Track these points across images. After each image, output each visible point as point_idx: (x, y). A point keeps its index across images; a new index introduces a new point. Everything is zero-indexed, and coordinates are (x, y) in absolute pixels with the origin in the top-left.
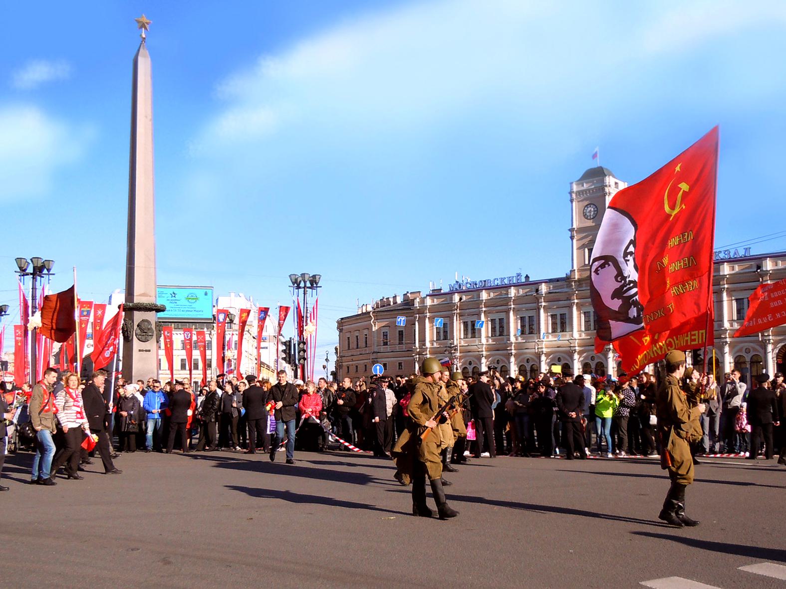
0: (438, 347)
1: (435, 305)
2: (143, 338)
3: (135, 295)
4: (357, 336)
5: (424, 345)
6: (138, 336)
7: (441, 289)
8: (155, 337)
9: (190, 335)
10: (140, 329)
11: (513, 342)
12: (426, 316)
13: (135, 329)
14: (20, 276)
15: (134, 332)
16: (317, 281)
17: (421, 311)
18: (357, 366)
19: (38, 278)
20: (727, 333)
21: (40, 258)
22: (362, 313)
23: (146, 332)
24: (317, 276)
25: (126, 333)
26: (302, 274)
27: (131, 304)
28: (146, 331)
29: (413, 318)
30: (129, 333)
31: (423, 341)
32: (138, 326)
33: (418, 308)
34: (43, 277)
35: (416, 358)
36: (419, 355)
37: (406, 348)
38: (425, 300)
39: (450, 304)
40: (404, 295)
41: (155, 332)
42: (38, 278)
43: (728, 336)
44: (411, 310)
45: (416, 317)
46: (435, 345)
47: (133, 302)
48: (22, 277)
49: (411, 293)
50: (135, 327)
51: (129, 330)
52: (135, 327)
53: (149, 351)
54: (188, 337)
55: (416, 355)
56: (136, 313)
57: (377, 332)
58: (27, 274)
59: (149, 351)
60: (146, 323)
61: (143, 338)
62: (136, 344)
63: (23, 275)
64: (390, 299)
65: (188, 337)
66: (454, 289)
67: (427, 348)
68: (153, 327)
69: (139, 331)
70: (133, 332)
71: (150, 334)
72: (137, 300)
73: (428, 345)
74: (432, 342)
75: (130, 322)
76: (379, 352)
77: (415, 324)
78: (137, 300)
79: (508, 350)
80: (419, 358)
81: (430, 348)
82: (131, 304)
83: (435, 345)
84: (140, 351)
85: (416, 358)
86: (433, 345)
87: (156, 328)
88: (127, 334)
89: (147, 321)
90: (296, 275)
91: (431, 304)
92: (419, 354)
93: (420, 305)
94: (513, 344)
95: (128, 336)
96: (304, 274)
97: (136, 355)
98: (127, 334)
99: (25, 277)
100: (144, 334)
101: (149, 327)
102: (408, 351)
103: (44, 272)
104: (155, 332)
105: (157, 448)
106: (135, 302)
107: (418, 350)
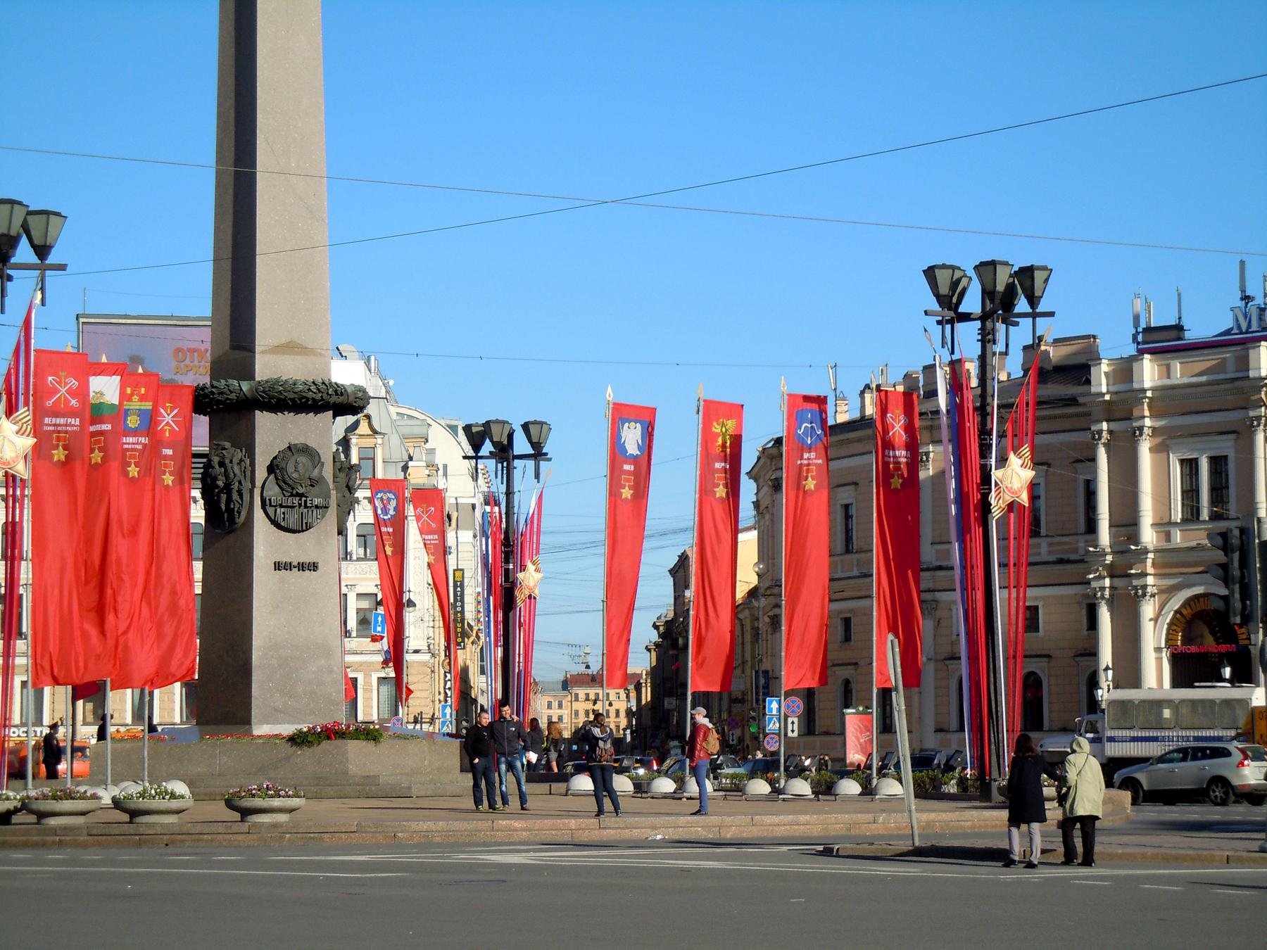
0: (1192, 549)
1: (1173, 387)
2: (293, 519)
3: (258, 349)
4: (846, 507)
5: (1134, 537)
6: (271, 511)
7: (1179, 328)
8: (332, 513)
9: (393, 503)
10: (285, 484)
11: (1150, 547)
12: (1141, 429)
13: (259, 483)
14: (939, 323)
15: (257, 492)
16: (1037, 294)
17: (1122, 409)
18: (847, 622)
19: (1000, 327)
20: (1149, 562)
21: (58, 214)
22: (863, 418)
23: (300, 495)
24: (1037, 273)
25: (224, 497)
26: (983, 264)
27: (245, 386)
28: (301, 490)
29: (1088, 435)
30: (235, 496)
31: (1127, 523)
32: (271, 469)
33: (1107, 397)
34: (1016, 324)
35: (1103, 589)
36: (1111, 576)
37: (1050, 553)
38: (1135, 365)
39: (1238, 384)
40: (1025, 348)
41: (333, 493)
42: (1000, 327)
43: (1150, 570)
44: (1080, 405)
45: (1100, 432)
46: (1178, 537)
47: (250, 376)
48: (948, 327)
49: (1056, 341)
50: (261, 473)
51: (235, 486)
52: (261, 473)
53: (314, 567)
54: (385, 511)
55: (1101, 578)
56: (263, 420)
57: (933, 484)
58: (966, 317)
59: (314, 567)
60: (302, 459)
61: (293, 519)
62: (266, 542)
63: (951, 322)
64: (968, 365)
65: (385, 511)
66: (1254, 327)
67: (1146, 551)
68: (328, 472)
69: (273, 492)
70: (252, 492)
71: (316, 501)
72: (269, 366)
73: (1148, 536)
74: (1164, 526)
75: (239, 454)
76: (940, 568)
77: (1093, 459)
78: (269, 366)
79: (1130, 575)
80: (1112, 588)
81: (1156, 551)
82: (245, 386)
83: (1178, 537)
84: (278, 566)
85: (1103, 589)
86: (1168, 537)
87: (335, 477)
88: (229, 500)
89: (306, 450)
90: (954, 268)
91: (1159, 383)
92: (1113, 572)
93: (1112, 389)
94: (1151, 555)
95: (230, 511)
96: (993, 264)
97: (265, 585)
98: (229, 500)
99: (958, 326)
100: (296, 501)
101: (315, 473)
102: (1061, 561)
103: (1017, 310)
104: (333, 493)
105: (1120, 788)
106: (258, 378)
107: (1109, 558)
